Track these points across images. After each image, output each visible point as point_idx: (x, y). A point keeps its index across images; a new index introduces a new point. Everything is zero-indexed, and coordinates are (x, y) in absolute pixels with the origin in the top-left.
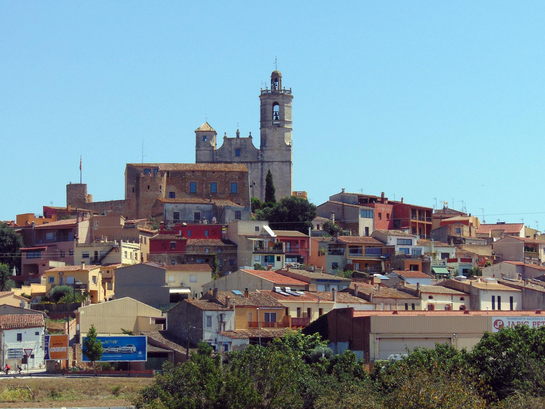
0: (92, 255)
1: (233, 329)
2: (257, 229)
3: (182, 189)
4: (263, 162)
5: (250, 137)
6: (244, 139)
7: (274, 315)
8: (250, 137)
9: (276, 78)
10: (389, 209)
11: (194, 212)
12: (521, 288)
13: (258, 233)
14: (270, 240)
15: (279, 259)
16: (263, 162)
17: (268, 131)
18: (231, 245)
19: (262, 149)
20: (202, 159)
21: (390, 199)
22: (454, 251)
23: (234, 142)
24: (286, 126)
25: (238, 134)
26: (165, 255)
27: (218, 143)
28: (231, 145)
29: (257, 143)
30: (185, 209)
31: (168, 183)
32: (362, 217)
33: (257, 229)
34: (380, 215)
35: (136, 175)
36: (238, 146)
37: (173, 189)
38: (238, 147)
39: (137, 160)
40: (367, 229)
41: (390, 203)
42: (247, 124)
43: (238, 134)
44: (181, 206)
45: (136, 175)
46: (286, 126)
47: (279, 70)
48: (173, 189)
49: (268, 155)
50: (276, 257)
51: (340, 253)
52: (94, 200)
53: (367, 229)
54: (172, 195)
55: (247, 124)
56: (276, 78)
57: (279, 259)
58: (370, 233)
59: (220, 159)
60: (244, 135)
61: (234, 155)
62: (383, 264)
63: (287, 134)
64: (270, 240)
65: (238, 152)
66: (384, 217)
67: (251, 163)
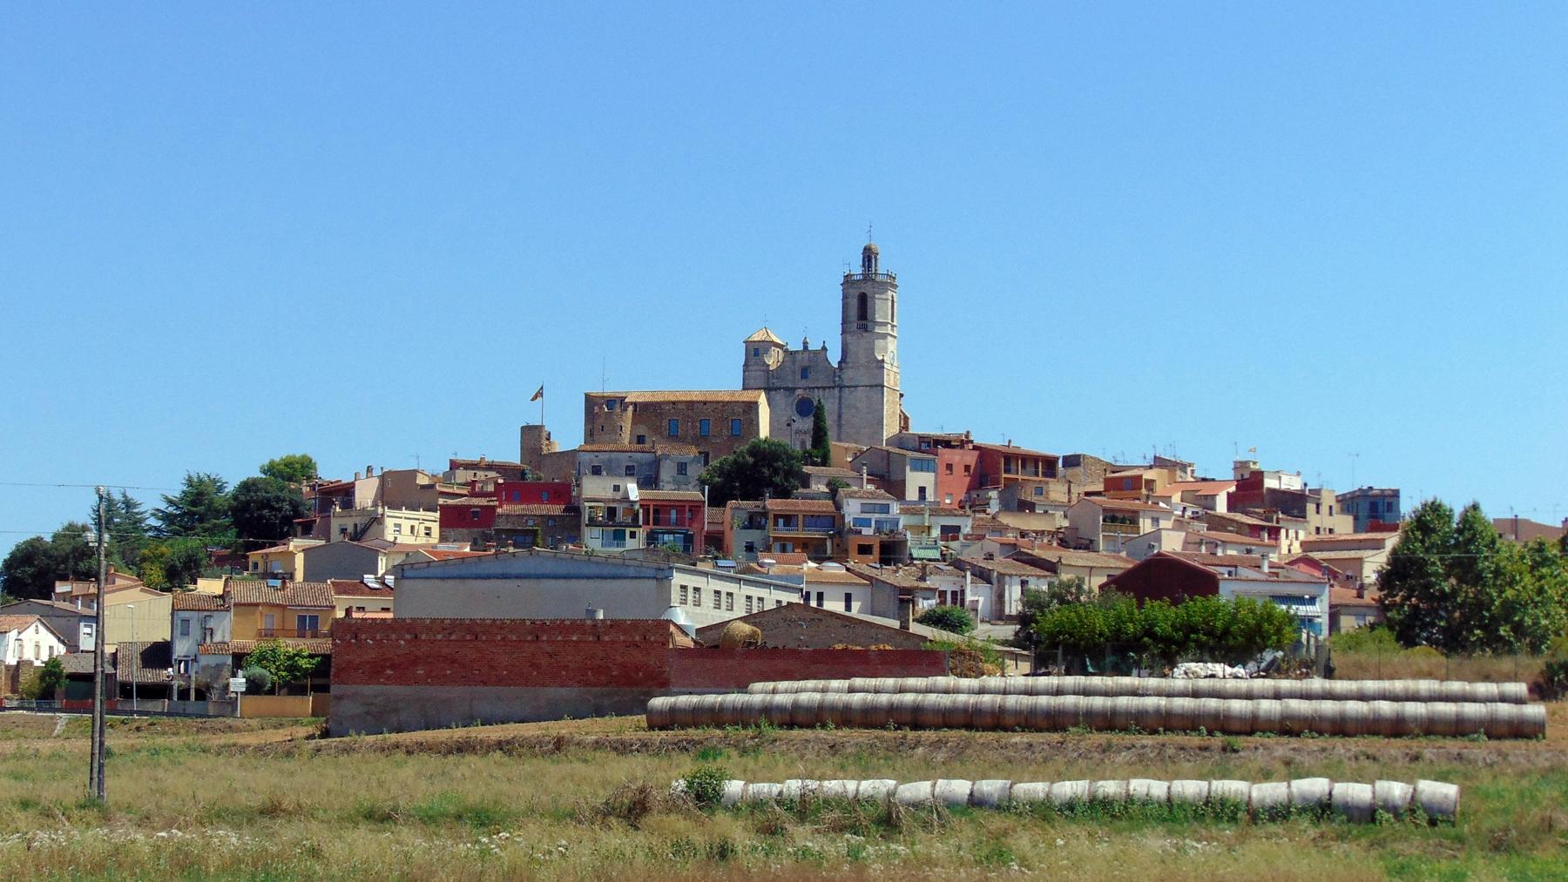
0: (350, 529)
1: (227, 639)
2: (617, 488)
3: (657, 430)
4: (841, 387)
5: (824, 349)
6: (815, 352)
7: (314, 619)
8: (824, 349)
9: (869, 256)
10: (971, 458)
11: (625, 464)
12: (870, 578)
13: (618, 496)
14: (627, 505)
15: (633, 535)
16: (841, 387)
17: (849, 337)
18: (574, 510)
19: (840, 368)
20: (752, 383)
21: (977, 442)
22: (970, 522)
23: (799, 357)
24: (878, 330)
25: (805, 344)
26: (465, 531)
27: (773, 360)
28: (794, 362)
29: (834, 357)
30: (610, 461)
31: (634, 423)
32: (914, 469)
33: (617, 488)
34: (949, 467)
35: (600, 411)
36: (806, 363)
37: (642, 430)
38: (806, 363)
39: (596, 390)
40: (922, 490)
41: (975, 448)
42: (822, 330)
43: (805, 344)
44: (602, 456)
45: (600, 411)
46: (878, 330)
47: (877, 246)
48: (642, 430)
49: (849, 375)
50: (628, 531)
51: (761, 527)
52: (558, 450)
53: (922, 490)
54: (641, 440)
55: (822, 330)
56: (869, 256)
57: (633, 535)
58: (930, 496)
59: (778, 384)
60: (814, 346)
61: (798, 376)
62: (829, 543)
63: (879, 343)
64: (627, 505)
65: (805, 372)
66: (959, 470)
67: (824, 388)
